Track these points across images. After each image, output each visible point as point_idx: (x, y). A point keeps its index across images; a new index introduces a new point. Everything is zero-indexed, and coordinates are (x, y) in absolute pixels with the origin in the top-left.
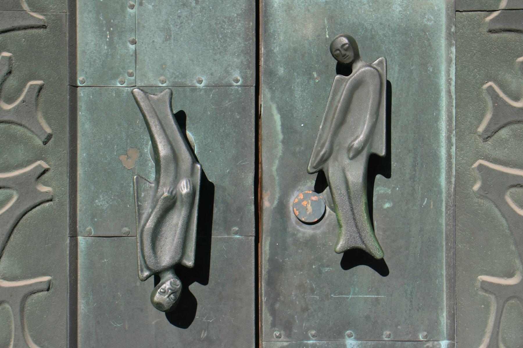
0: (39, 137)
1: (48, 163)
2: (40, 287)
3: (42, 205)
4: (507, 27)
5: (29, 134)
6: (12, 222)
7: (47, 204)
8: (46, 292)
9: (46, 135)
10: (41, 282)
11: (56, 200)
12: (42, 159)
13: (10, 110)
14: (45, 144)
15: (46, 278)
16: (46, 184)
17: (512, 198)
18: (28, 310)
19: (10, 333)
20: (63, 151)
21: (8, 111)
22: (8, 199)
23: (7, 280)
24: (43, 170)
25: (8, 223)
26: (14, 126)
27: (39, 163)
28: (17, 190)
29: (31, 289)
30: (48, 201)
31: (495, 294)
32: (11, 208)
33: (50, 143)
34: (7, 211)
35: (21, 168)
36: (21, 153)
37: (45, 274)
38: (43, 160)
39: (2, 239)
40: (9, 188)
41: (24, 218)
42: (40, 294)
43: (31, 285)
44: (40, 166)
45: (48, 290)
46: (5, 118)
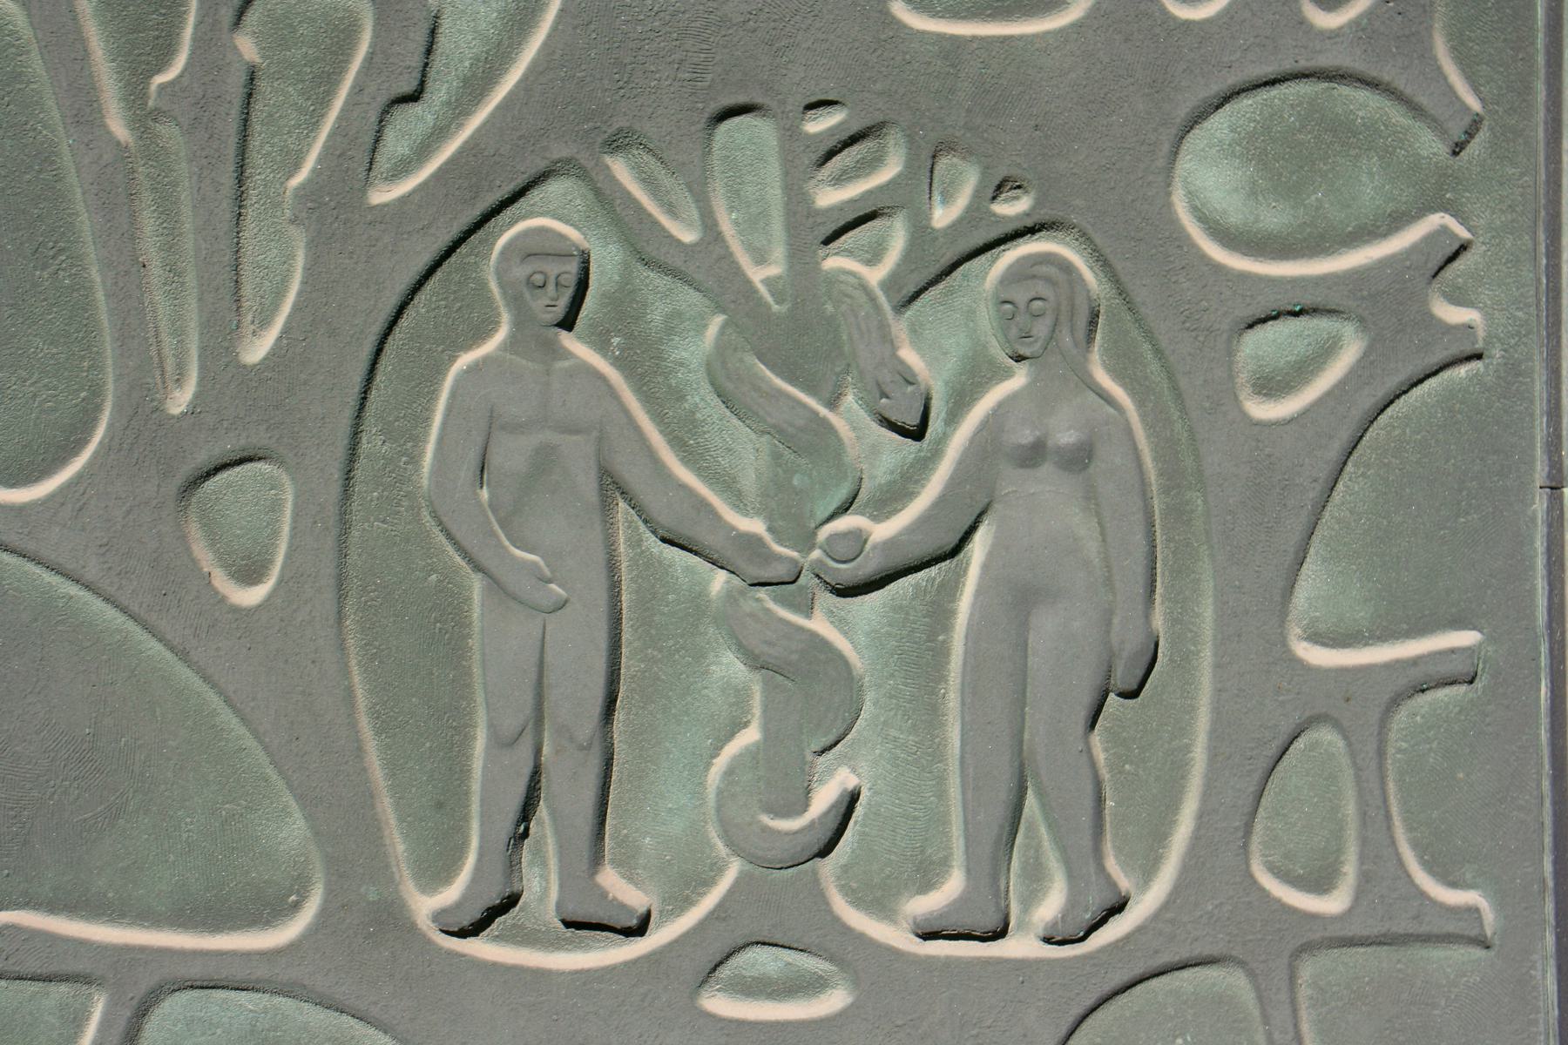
0: (1436, 125)
1: (1463, 221)
2: (1446, 669)
3: (1445, 375)
4: (1216, 87)
5: (1397, 116)
6: (1344, 435)
7: (1462, 371)
8: (1464, 688)
9: (1467, 120)
10: (1453, 651)
11: (1497, 353)
12: (1445, 207)
13: (1341, 28)
14: (1455, 153)
15: (1466, 638)
16: (1458, 298)
17: (1317, 638)
18: (1399, 751)
19: (1338, 835)
20: (1522, 174)
21: (1333, 35)
22: (1326, 351)
23: (1324, 645)
24: (1455, 247)
25: (1331, 437)
26: (1344, 90)
27: (1436, 220)
28: (1362, 320)
29: (1416, 674)
30: (1469, 358)
31: (1241, 964)
32: (1341, 385)
33: (1475, 148)
34: (1329, 394)
35: (1367, 242)
36: (1370, 189)
37: (1458, 623)
38: (1446, 211)
39: (1311, 495)
40: (1330, 312)
41: (1383, 418)
42: (1442, 694)
43: (1415, 661)
44: (1444, 230)
45: (1471, 682)
46: (1324, 61)
